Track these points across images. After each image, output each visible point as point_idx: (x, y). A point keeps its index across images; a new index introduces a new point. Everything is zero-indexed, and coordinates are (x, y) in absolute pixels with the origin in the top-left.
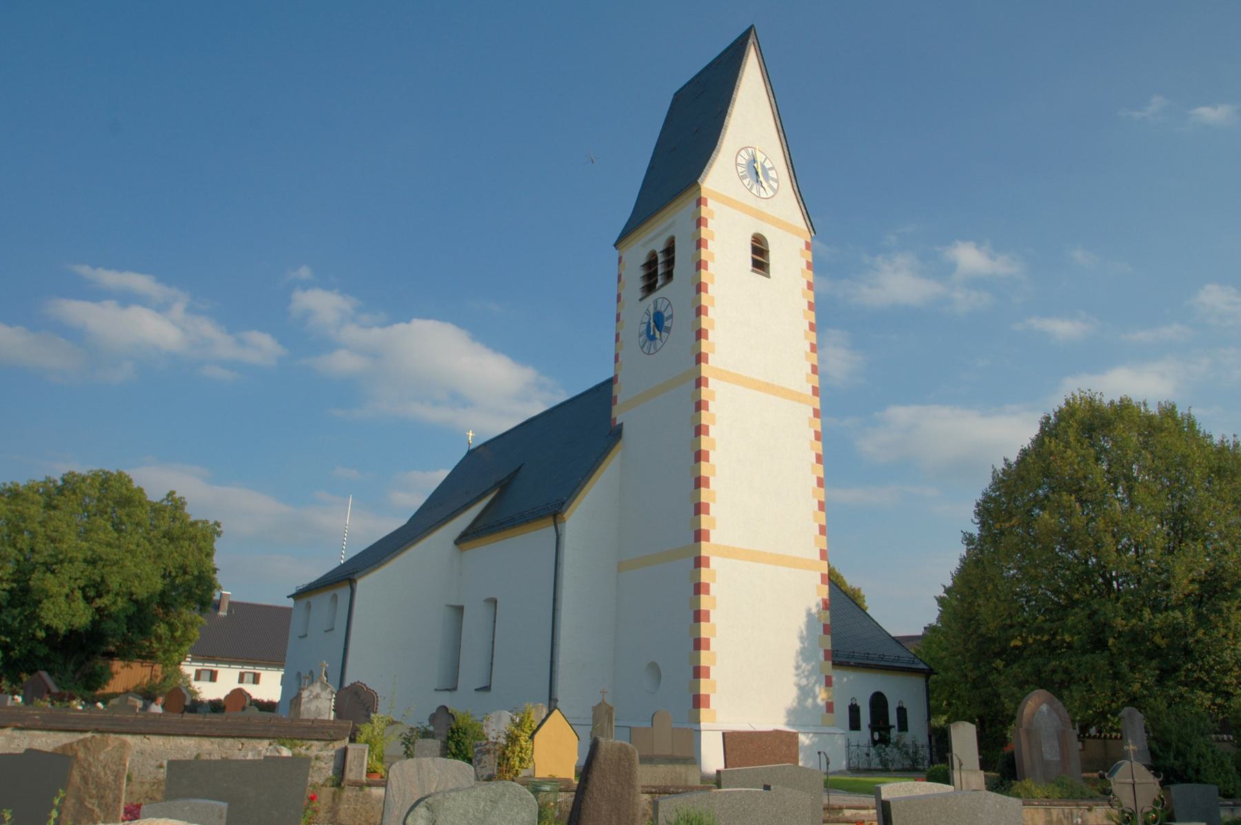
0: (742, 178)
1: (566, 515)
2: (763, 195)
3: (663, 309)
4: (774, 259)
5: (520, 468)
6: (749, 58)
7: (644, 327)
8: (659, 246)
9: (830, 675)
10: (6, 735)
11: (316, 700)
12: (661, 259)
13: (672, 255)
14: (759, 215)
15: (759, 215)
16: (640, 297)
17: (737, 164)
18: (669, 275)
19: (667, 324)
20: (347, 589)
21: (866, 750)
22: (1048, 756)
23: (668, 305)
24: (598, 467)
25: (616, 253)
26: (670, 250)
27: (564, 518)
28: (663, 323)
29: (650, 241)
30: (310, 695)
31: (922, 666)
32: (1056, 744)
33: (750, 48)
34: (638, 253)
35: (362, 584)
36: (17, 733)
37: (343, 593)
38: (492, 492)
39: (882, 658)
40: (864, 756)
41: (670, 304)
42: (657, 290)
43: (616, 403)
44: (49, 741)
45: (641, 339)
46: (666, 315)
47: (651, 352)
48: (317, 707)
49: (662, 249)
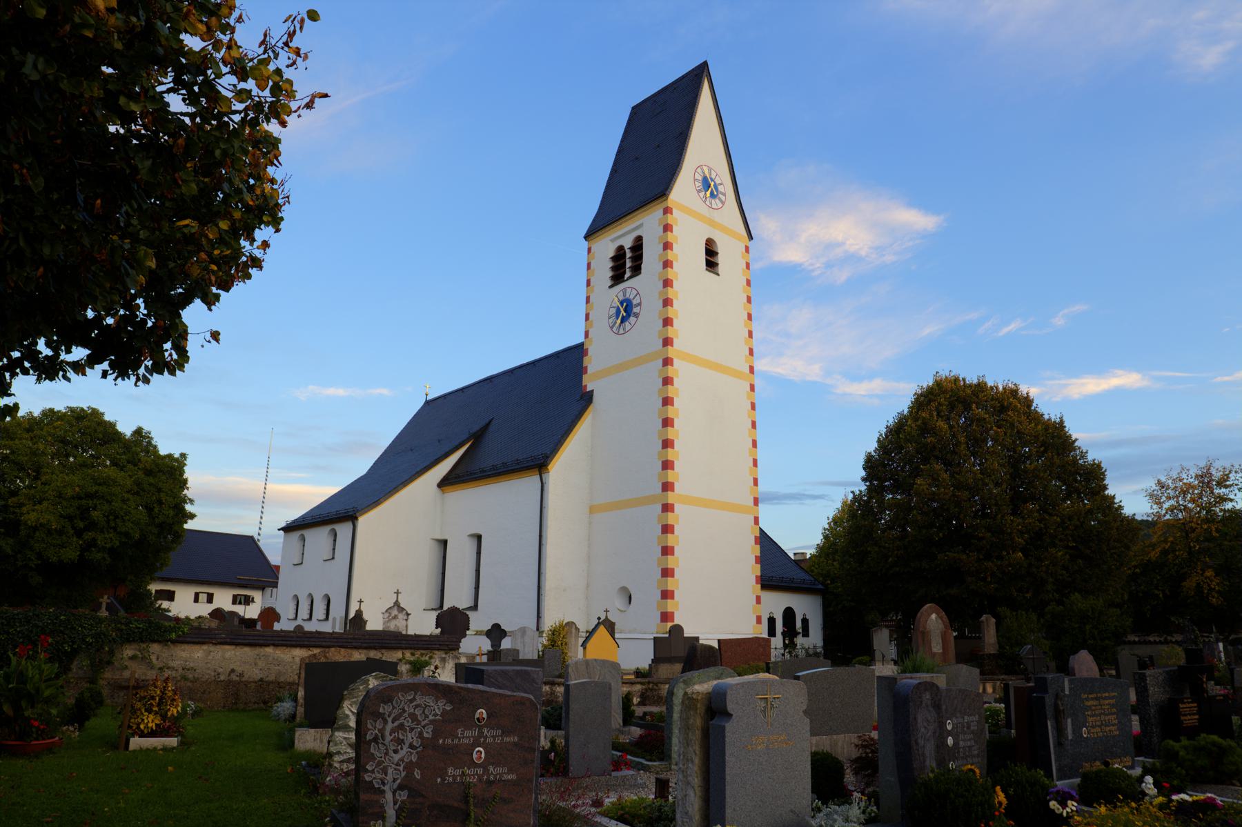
0: (699, 191)
1: (549, 467)
2: (714, 206)
3: (631, 297)
4: (721, 259)
5: (490, 421)
6: (703, 89)
7: (613, 311)
8: (628, 243)
9: (759, 595)
10: (203, 650)
11: (394, 620)
12: (629, 254)
13: (640, 252)
14: (712, 223)
15: (712, 223)
16: (610, 284)
17: (695, 180)
18: (637, 270)
19: (636, 310)
20: (349, 526)
21: (782, 651)
22: (935, 650)
23: (636, 296)
24: (574, 426)
25: (585, 244)
26: (638, 246)
27: (548, 469)
28: (632, 310)
29: (621, 236)
30: (389, 616)
31: (820, 586)
32: (940, 641)
33: (704, 81)
34: (606, 246)
35: (365, 521)
36: (212, 648)
37: (344, 530)
38: (467, 443)
39: (792, 580)
40: (781, 656)
41: (638, 293)
42: (624, 281)
43: (586, 372)
44: (237, 654)
45: (611, 320)
46: (635, 302)
47: (620, 332)
48: (396, 625)
49: (629, 246)
